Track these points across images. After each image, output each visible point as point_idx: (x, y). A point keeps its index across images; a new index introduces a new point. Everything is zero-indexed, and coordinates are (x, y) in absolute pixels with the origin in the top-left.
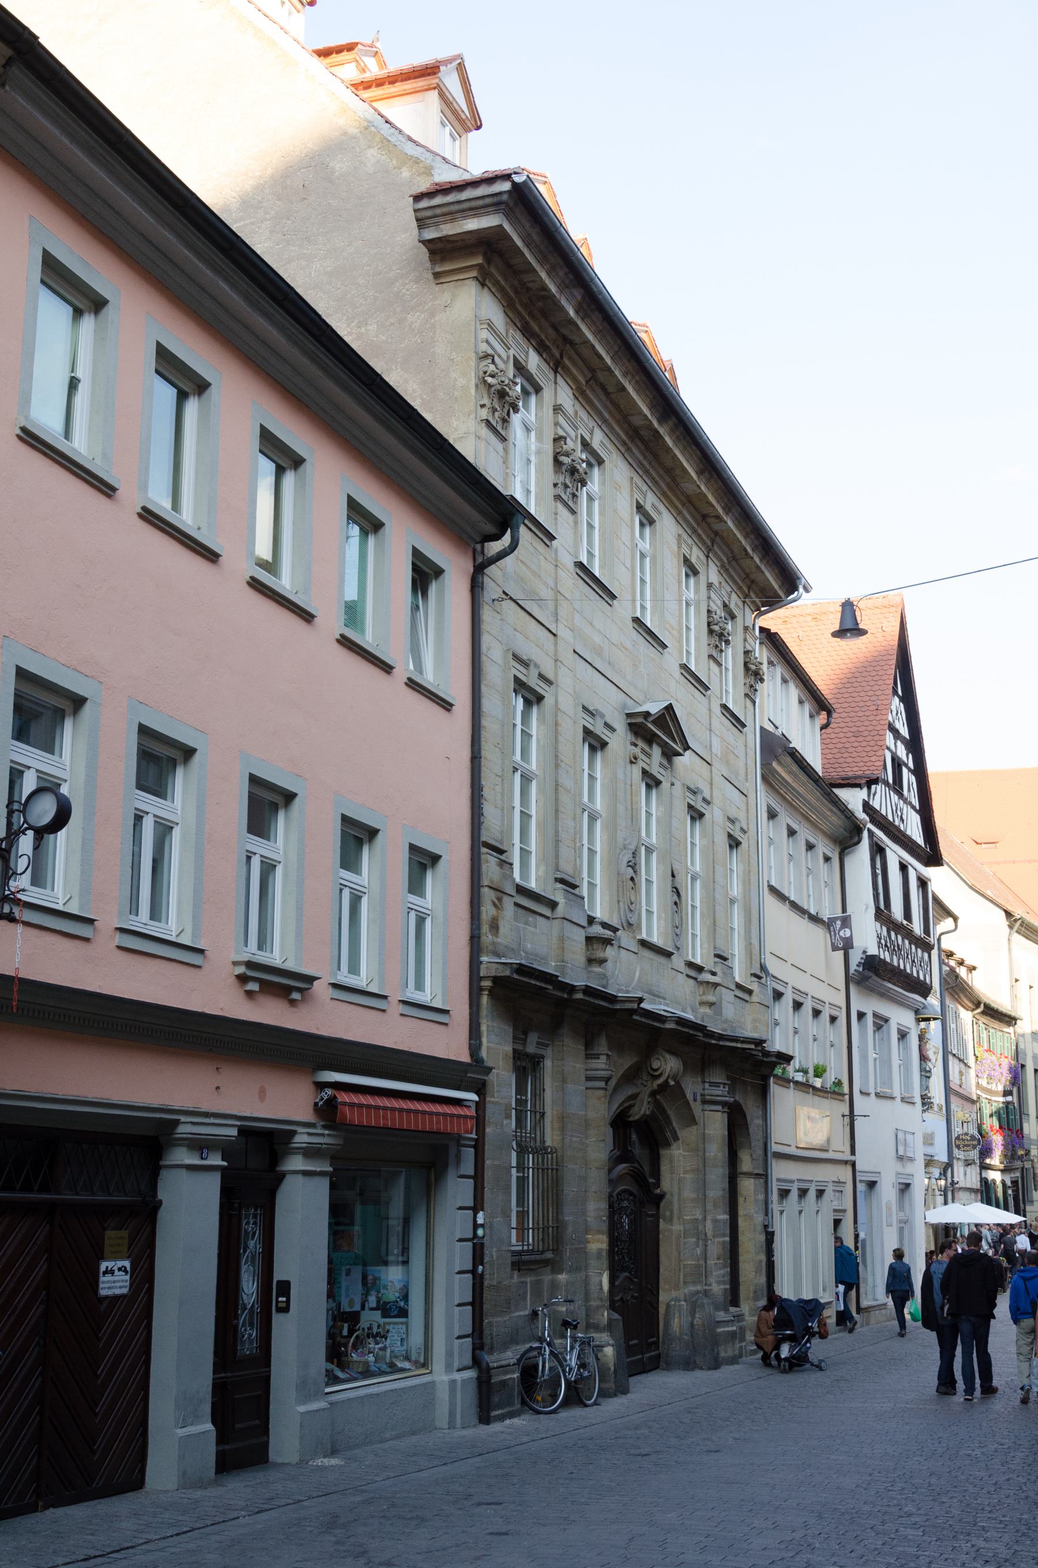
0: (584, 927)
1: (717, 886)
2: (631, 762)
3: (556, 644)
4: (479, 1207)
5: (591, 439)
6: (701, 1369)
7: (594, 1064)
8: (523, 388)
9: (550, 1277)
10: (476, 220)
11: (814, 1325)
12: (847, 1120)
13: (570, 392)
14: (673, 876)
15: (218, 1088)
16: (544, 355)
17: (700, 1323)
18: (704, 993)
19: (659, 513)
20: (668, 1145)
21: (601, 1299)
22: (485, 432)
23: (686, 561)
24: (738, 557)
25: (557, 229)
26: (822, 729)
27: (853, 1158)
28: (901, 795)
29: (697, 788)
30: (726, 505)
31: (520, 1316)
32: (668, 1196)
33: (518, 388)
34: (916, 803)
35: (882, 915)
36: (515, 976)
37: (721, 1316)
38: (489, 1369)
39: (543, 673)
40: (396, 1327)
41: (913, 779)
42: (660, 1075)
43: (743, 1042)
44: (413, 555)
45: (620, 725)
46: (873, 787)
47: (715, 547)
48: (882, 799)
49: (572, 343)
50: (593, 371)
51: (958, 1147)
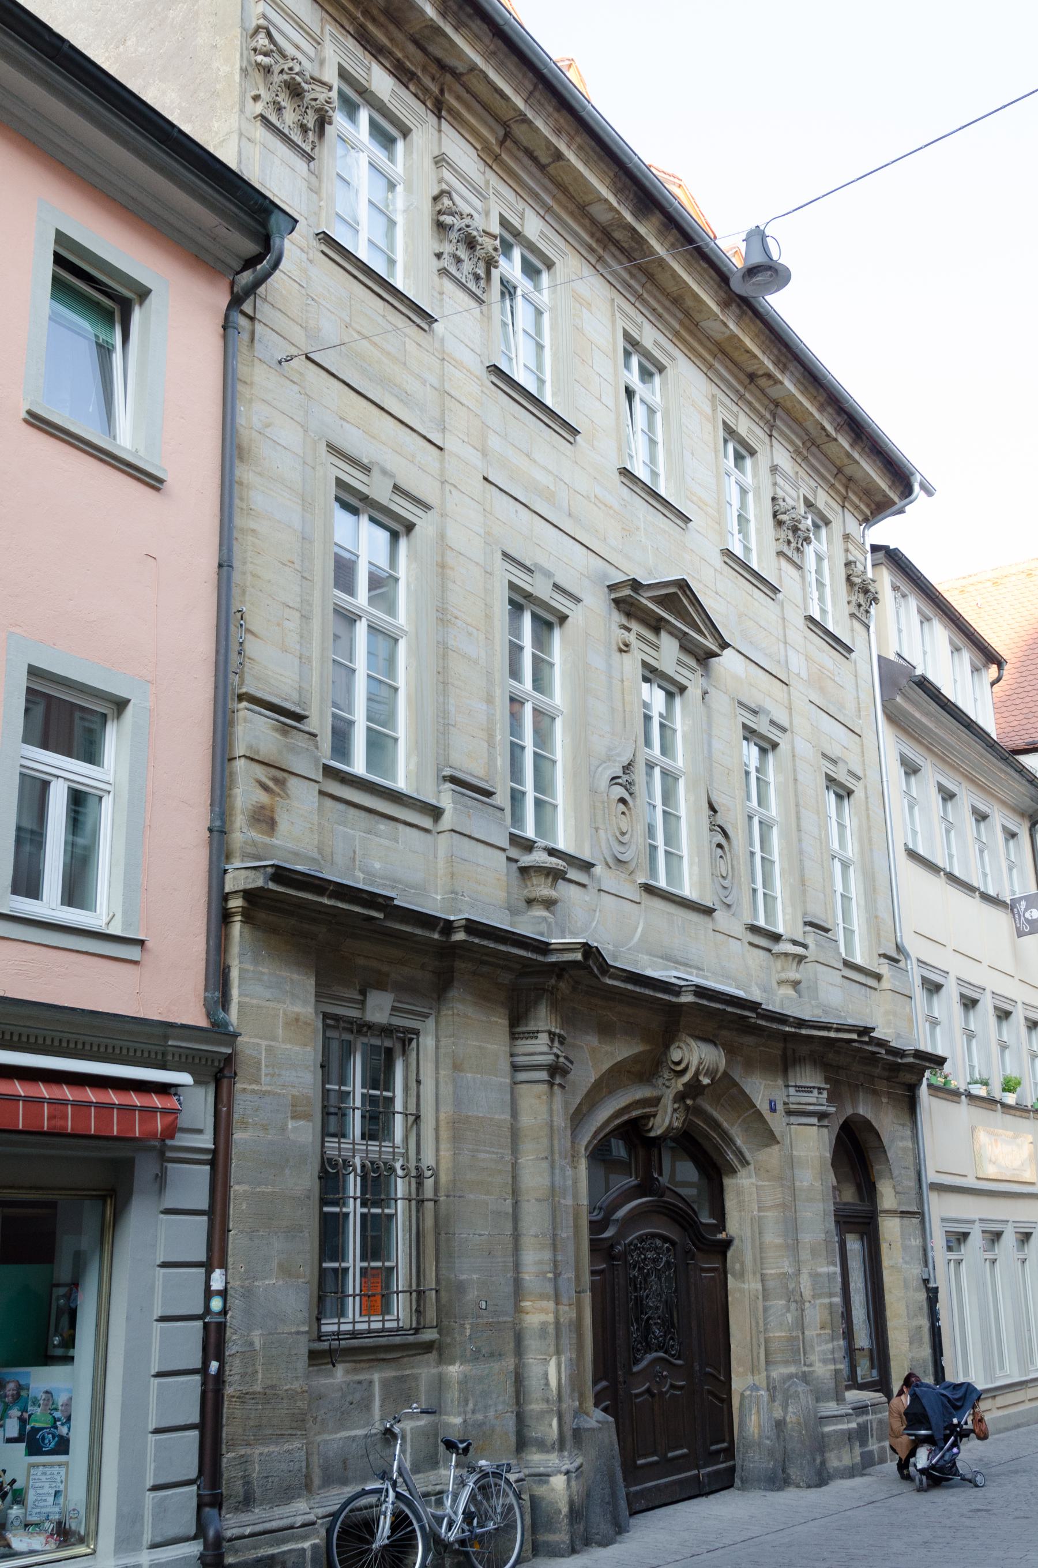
0: (504, 850)
3: (442, 461)
4: (216, 1262)
5: (815, 499)
6: (798, 1486)
7: (526, 1046)
8: (813, 522)
9: (434, 1371)
11: (968, 1420)
14: (712, 808)
17: (794, 1419)
18: (783, 970)
20: (733, 1171)
21: (547, 1401)
22: (260, 132)
23: (730, 432)
24: (819, 442)
29: (759, 707)
30: (779, 361)
31: (354, 1438)
32: (736, 1242)
33: (809, 522)
36: (272, 886)
37: (831, 1408)
38: (219, 1539)
39: (775, 719)
40: (48, 1470)
43: (838, 1030)
49: (456, 75)
50: (505, 125)
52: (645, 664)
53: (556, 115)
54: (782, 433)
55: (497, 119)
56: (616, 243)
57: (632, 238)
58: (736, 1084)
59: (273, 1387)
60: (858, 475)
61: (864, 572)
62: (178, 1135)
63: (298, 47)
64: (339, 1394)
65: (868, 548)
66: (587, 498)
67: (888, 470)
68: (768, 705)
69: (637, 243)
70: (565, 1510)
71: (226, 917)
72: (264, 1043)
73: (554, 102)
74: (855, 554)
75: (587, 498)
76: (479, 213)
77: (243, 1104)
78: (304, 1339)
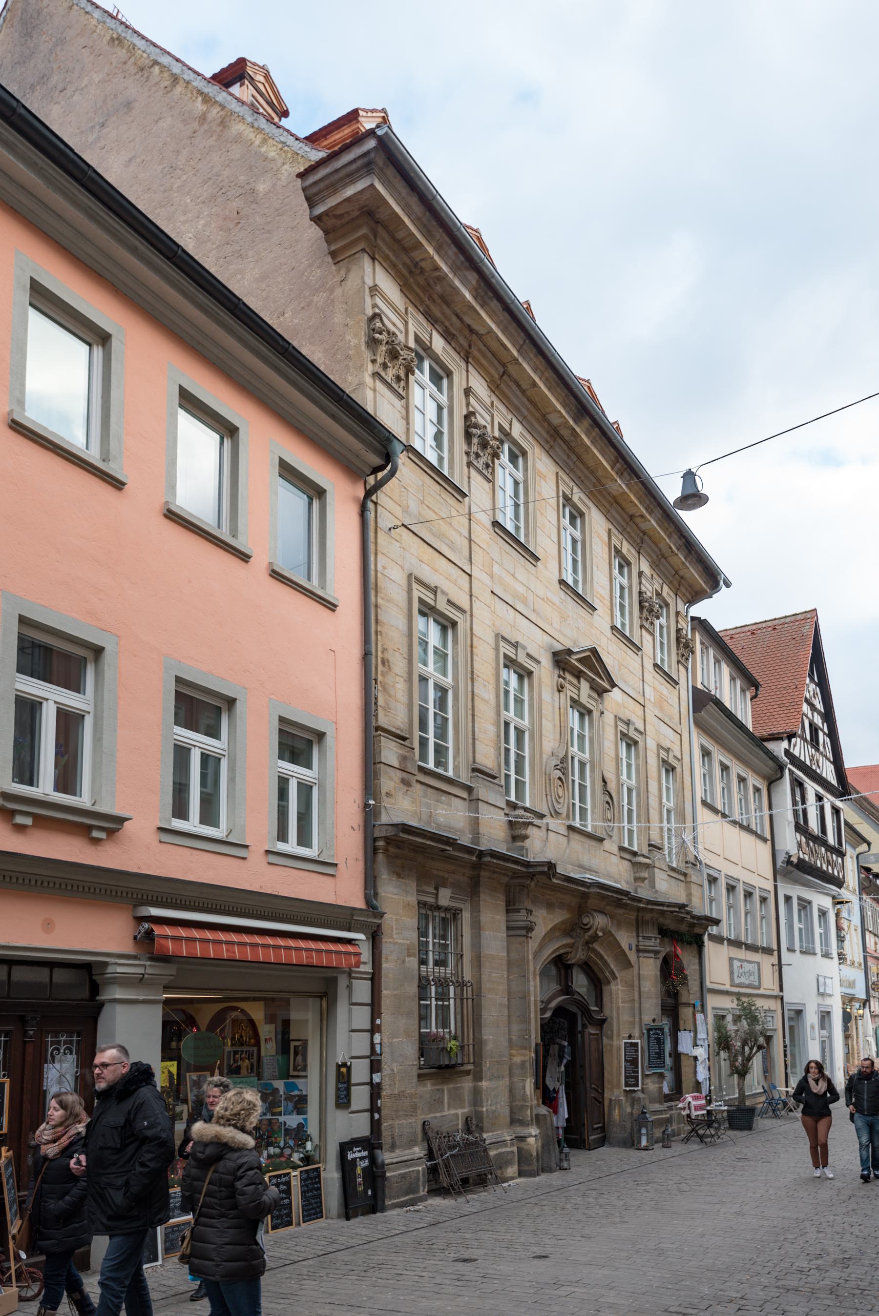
1: (650, 795)
2: (559, 691)
5: (510, 429)
10: (352, 186)
12: (776, 968)
14: (604, 781)
19: (589, 508)
20: (609, 983)
24: (666, 555)
25: (434, 197)
26: (751, 699)
27: (781, 994)
28: (817, 750)
32: (609, 1020)
34: (830, 755)
35: (801, 828)
41: (828, 740)
42: (590, 928)
44: (280, 465)
45: (546, 662)
46: (793, 740)
48: (800, 749)
51: (873, 989)
53: (535, 360)
54: (645, 551)
55: (500, 362)
56: (562, 438)
57: (572, 434)
58: (612, 935)
59: (403, 1092)
60: (687, 576)
61: (687, 635)
62: (362, 966)
63: (394, 324)
64: (428, 1096)
66: (543, 599)
68: (634, 719)
69: (574, 437)
70: (535, 1154)
71: (375, 850)
72: (394, 917)
73: (535, 351)
74: (682, 624)
75: (543, 599)
78: (415, 1068)
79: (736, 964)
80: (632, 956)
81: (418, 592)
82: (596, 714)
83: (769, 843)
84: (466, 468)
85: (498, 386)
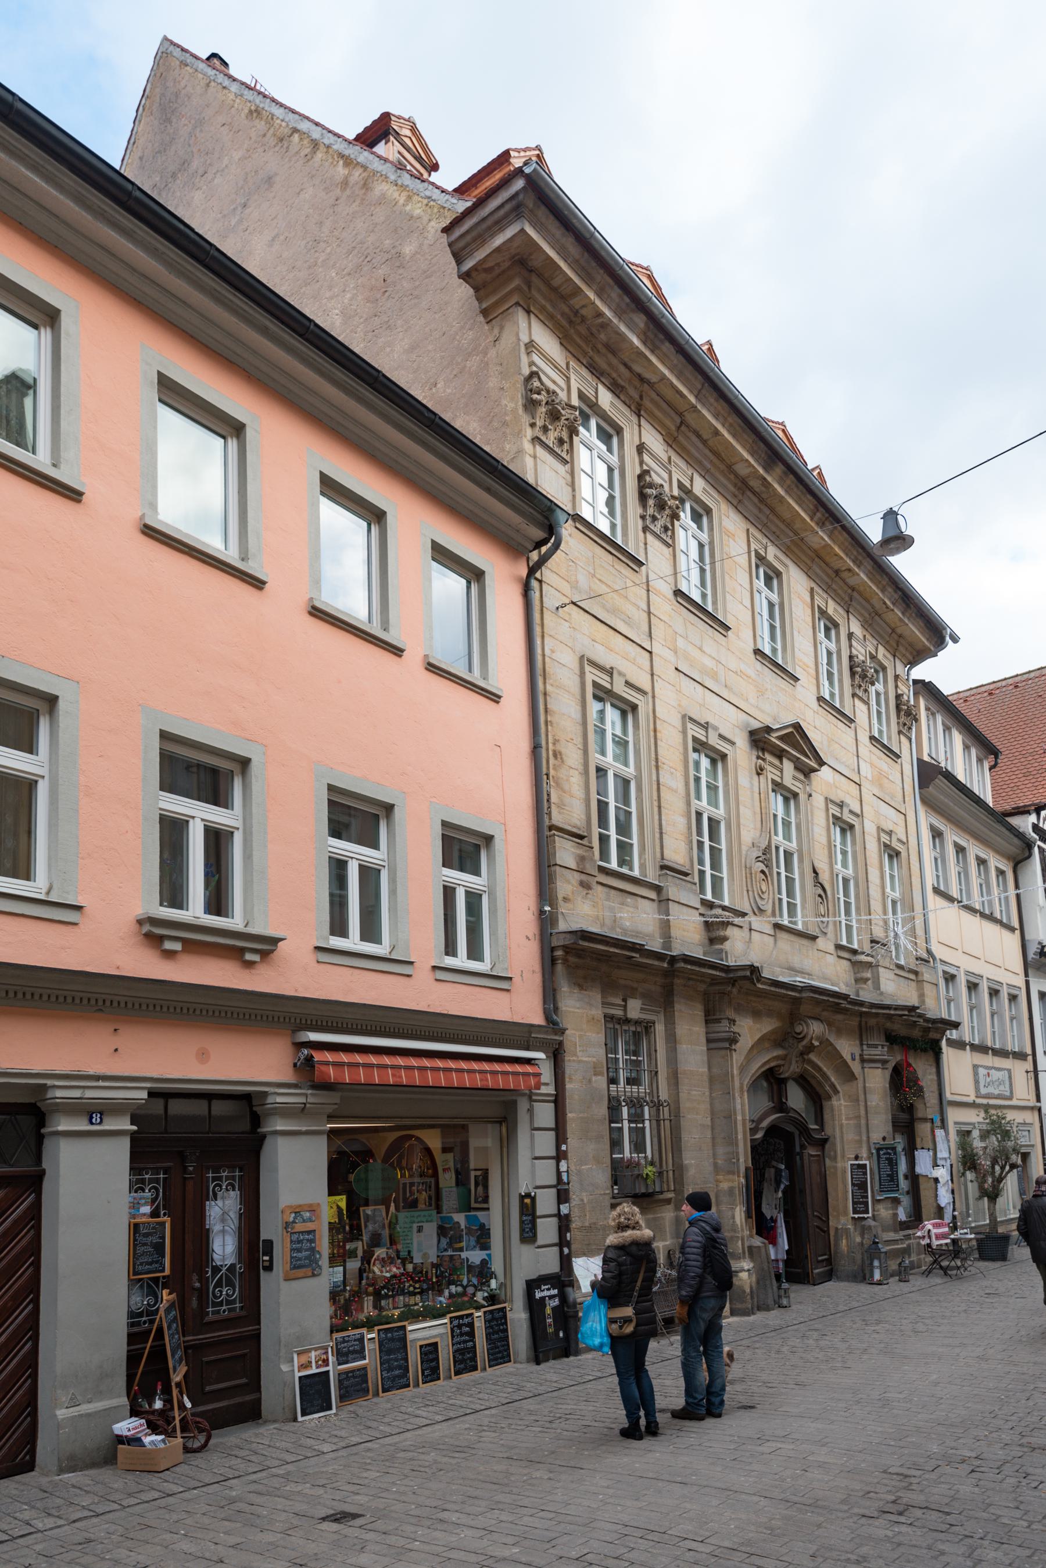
2: (758, 774)
5: (692, 486)
12: (1032, 1075)
13: (858, 624)
14: (815, 872)
15: (116, 1050)
16: (622, 397)
19: (786, 566)
20: (829, 1098)
27: (1038, 1104)
32: (831, 1139)
43: (896, 1009)
45: (742, 742)
47: (534, 293)
52: (773, 781)
53: (715, 404)
54: (855, 609)
58: (831, 1044)
59: (595, 1224)
61: (908, 701)
62: (543, 1087)
63: (554, 382)
65: (911, 683)
67: (928, 628)
68: (848, 800)
69: (766, 487)
70: (748, 1290)
71: (553, 961)
73: (715, 394)
74: (903, 689)
75: (736, 673)
76: (562, 390)
77: (570, 1067)
78: (608, 1198)
79: (982, 1072)
80: (856, 1067)
81: (592, 675)
82: (802, 797)
83: (1018, 932)
84: (641, 534)
85: (675, 439)
